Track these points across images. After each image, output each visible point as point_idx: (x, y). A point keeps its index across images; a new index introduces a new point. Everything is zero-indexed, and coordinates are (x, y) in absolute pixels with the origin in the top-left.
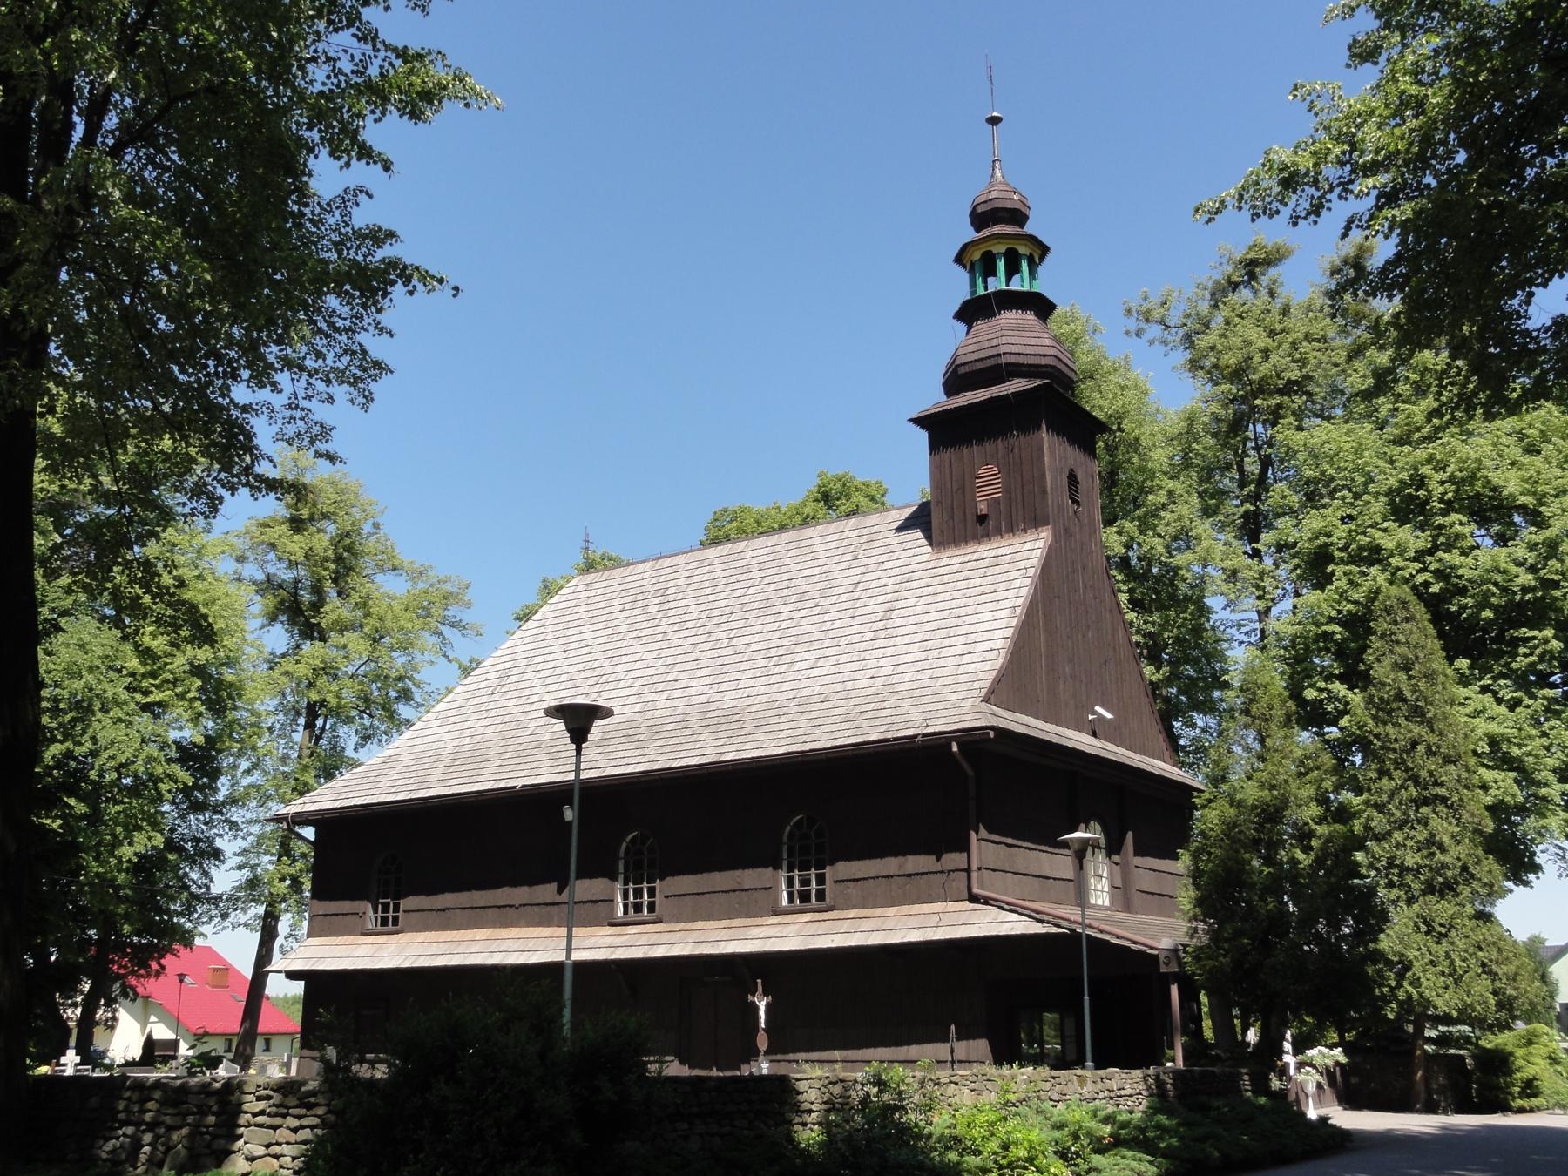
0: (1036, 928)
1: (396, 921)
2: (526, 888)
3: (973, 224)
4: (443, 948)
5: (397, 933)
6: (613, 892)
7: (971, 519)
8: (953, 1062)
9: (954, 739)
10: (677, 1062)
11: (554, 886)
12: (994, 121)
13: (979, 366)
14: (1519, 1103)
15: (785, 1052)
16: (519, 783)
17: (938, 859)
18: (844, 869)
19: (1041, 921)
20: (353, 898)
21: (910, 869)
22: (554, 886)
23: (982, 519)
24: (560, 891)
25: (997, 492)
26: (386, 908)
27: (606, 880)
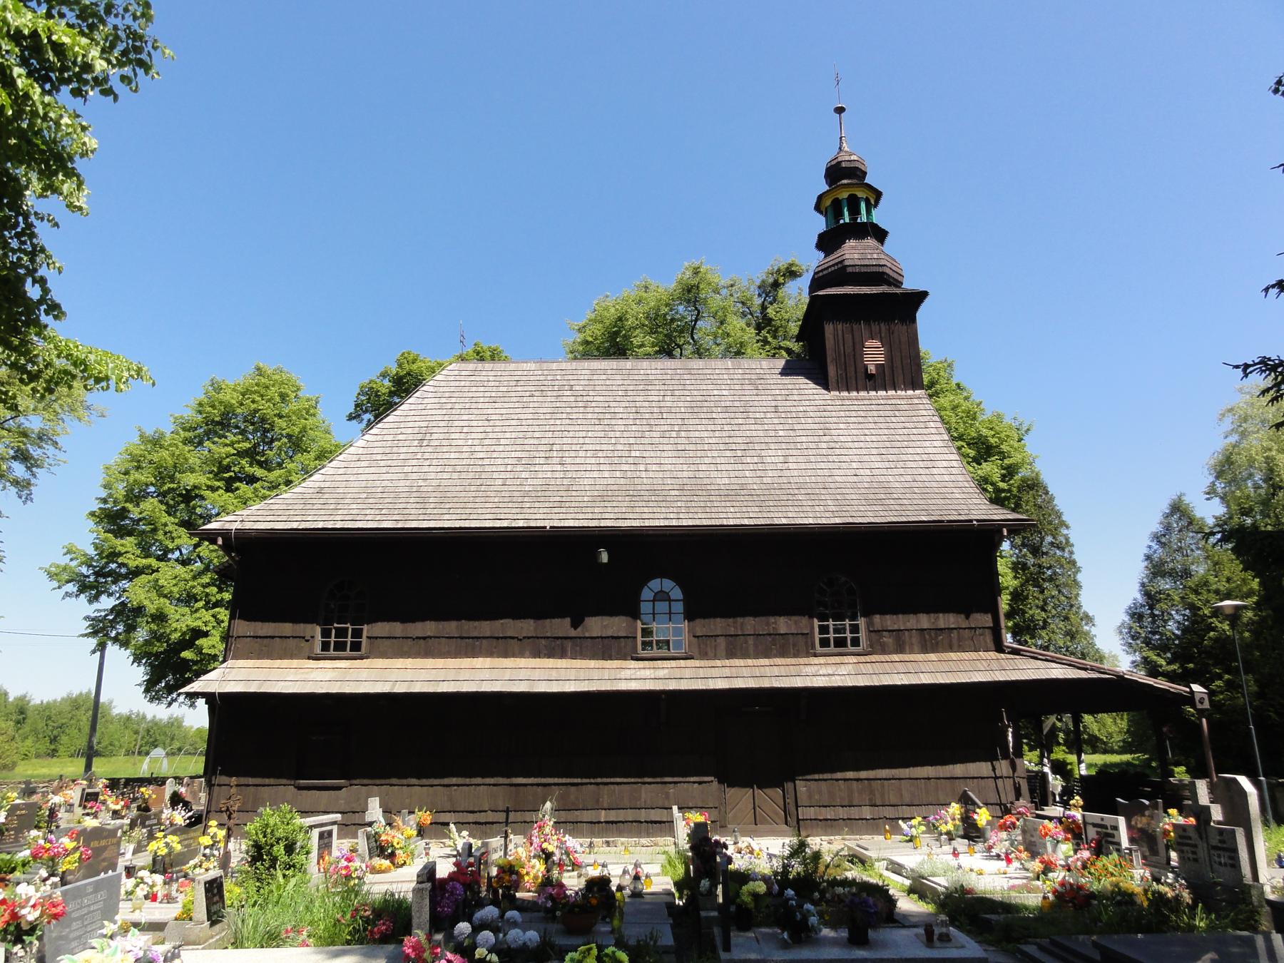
0: (1083, 675)
1: (356, 647)
2: (532, 622)
3: (826, 176)
4: (374, 675)
5: (361, 658)
6: (314, 631)
7: (861, 375)
8: (996, 778)
9: (219, 534)
10: (715, 783)
11: (568, 620)
12: (840, 110)
13: (863, 270)
14: (810, 813)
15: (833, 771)
16: (548, 524)
17: (967, 617)
18: (381, 628)
19: (1085, 669)
20: (295, 620)
21: (260, 633)
22: (568, 620)
23: (870, 377)
24: (575, 625)
25: (881, 360)
26: (341, 633)
27: (629, 619)
